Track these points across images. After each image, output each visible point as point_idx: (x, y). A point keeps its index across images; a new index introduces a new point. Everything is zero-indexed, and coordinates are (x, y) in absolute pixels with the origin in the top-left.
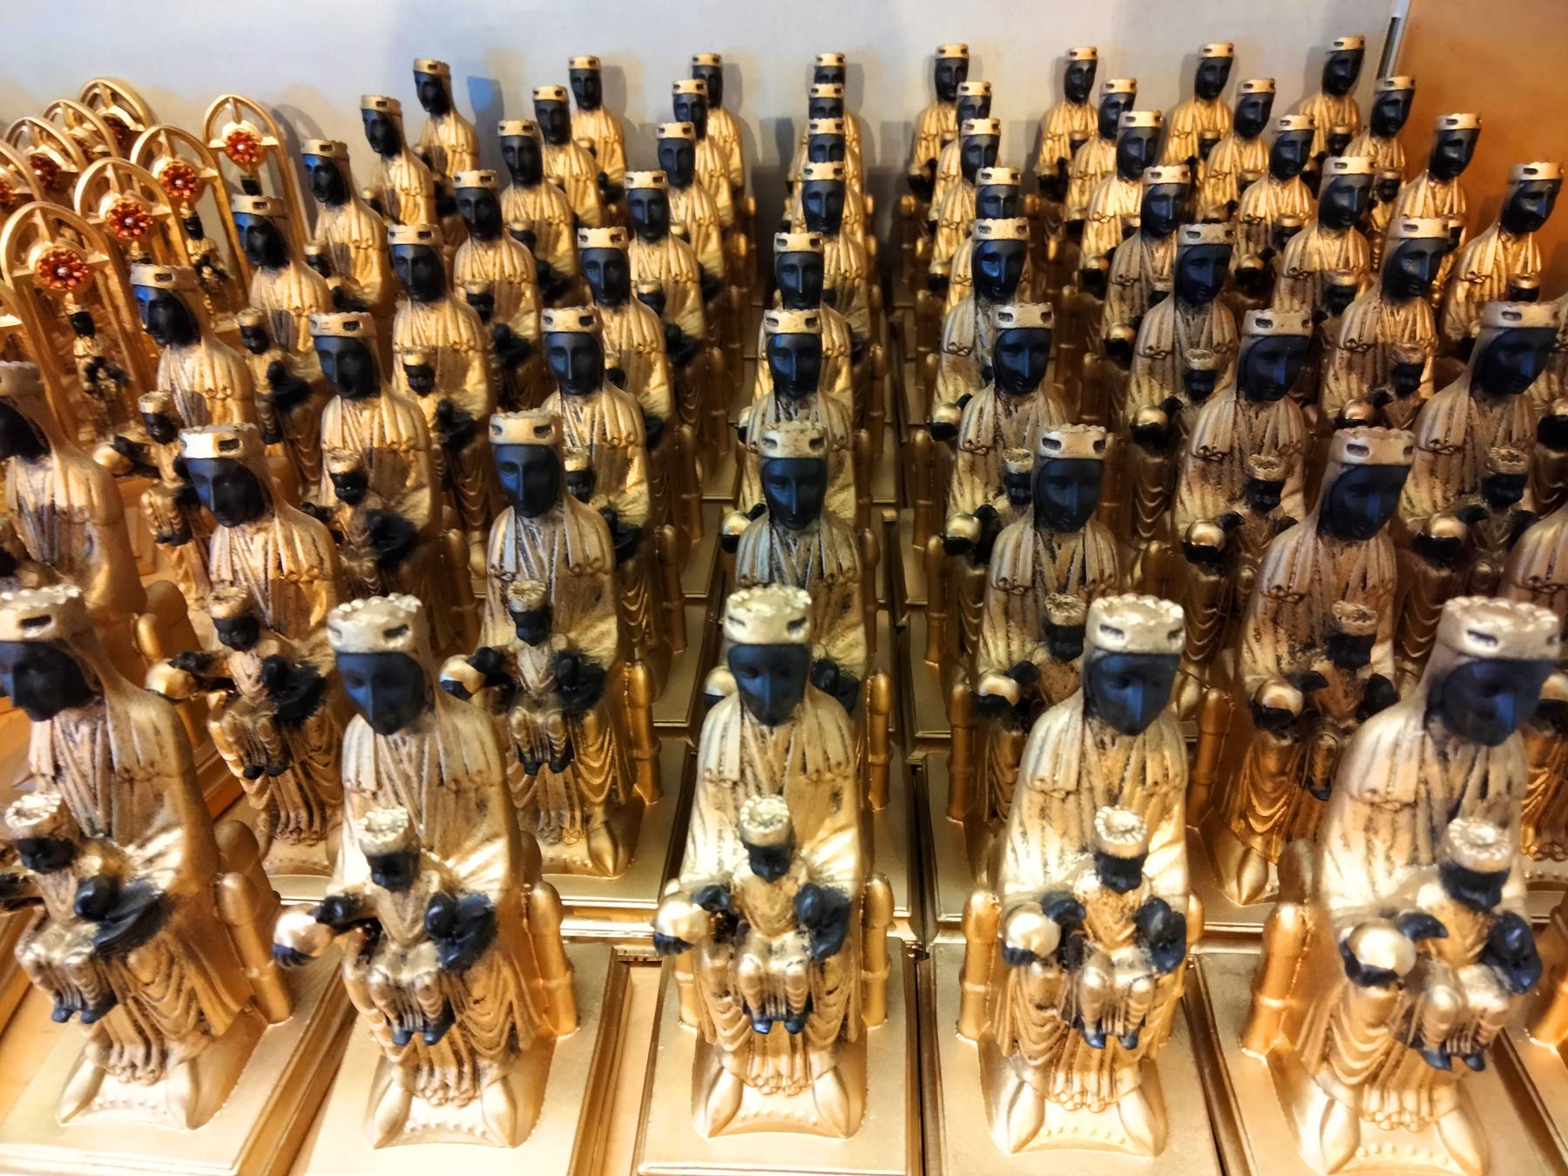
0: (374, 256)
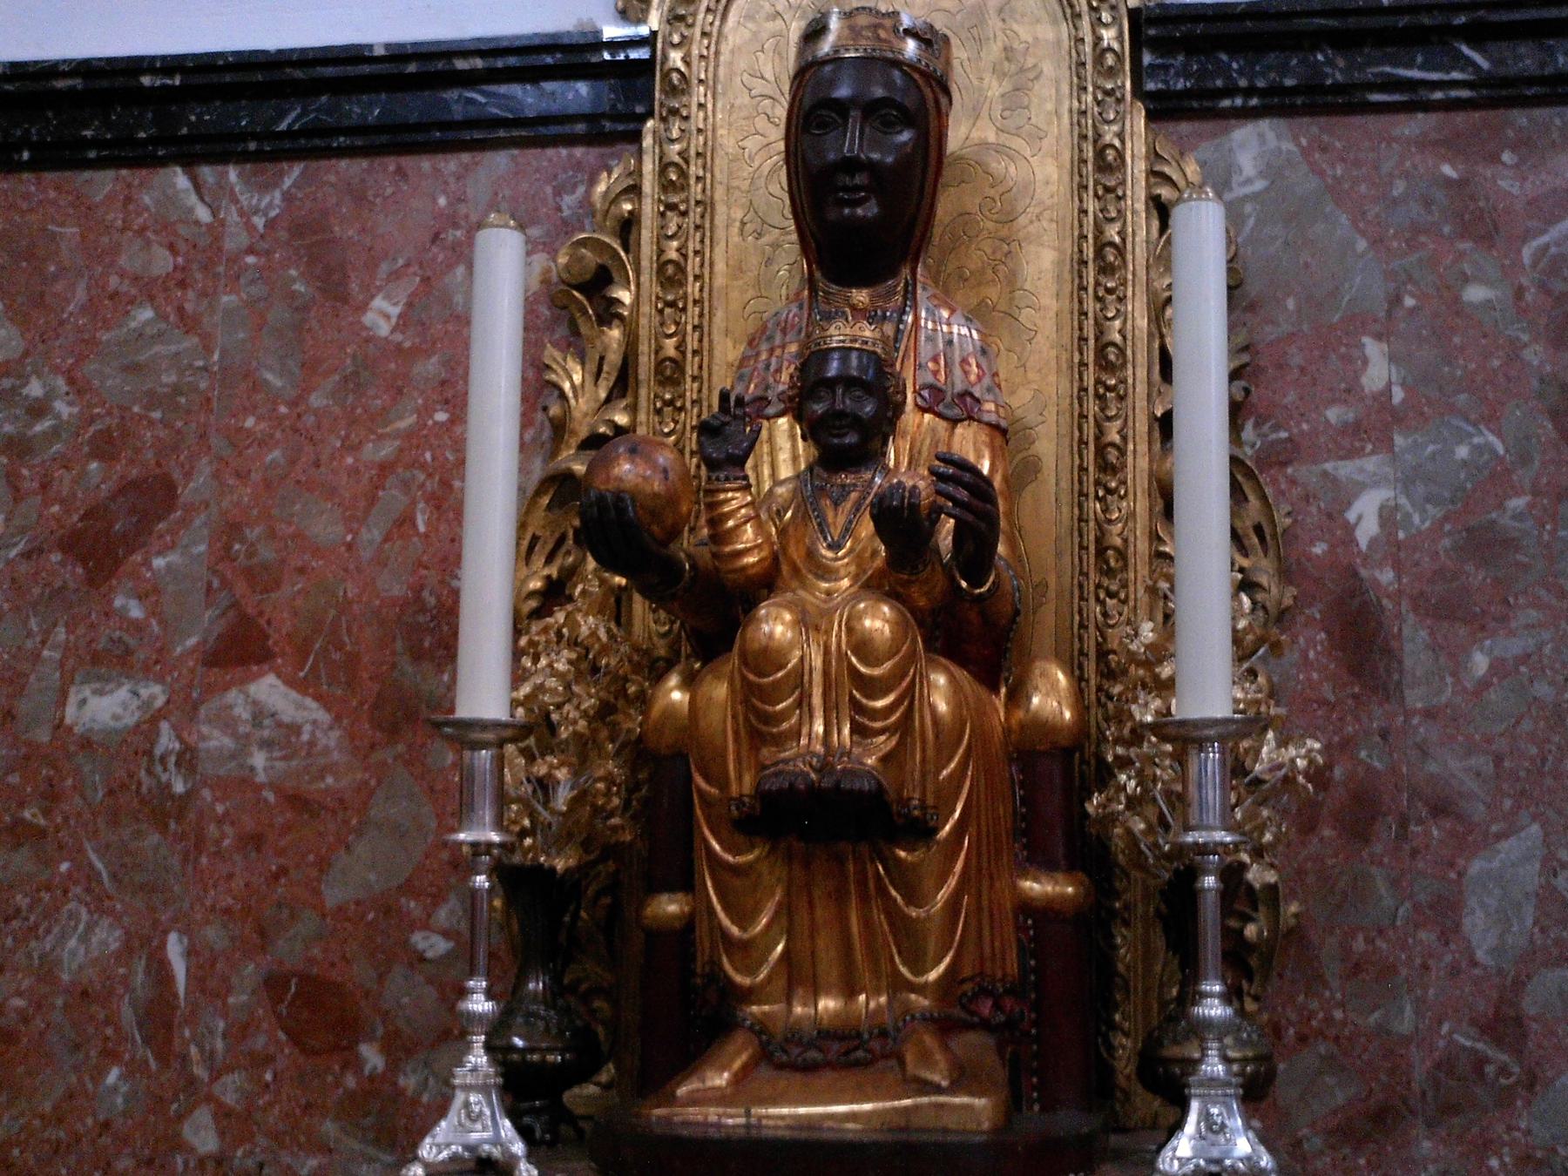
0: (1014, 946)
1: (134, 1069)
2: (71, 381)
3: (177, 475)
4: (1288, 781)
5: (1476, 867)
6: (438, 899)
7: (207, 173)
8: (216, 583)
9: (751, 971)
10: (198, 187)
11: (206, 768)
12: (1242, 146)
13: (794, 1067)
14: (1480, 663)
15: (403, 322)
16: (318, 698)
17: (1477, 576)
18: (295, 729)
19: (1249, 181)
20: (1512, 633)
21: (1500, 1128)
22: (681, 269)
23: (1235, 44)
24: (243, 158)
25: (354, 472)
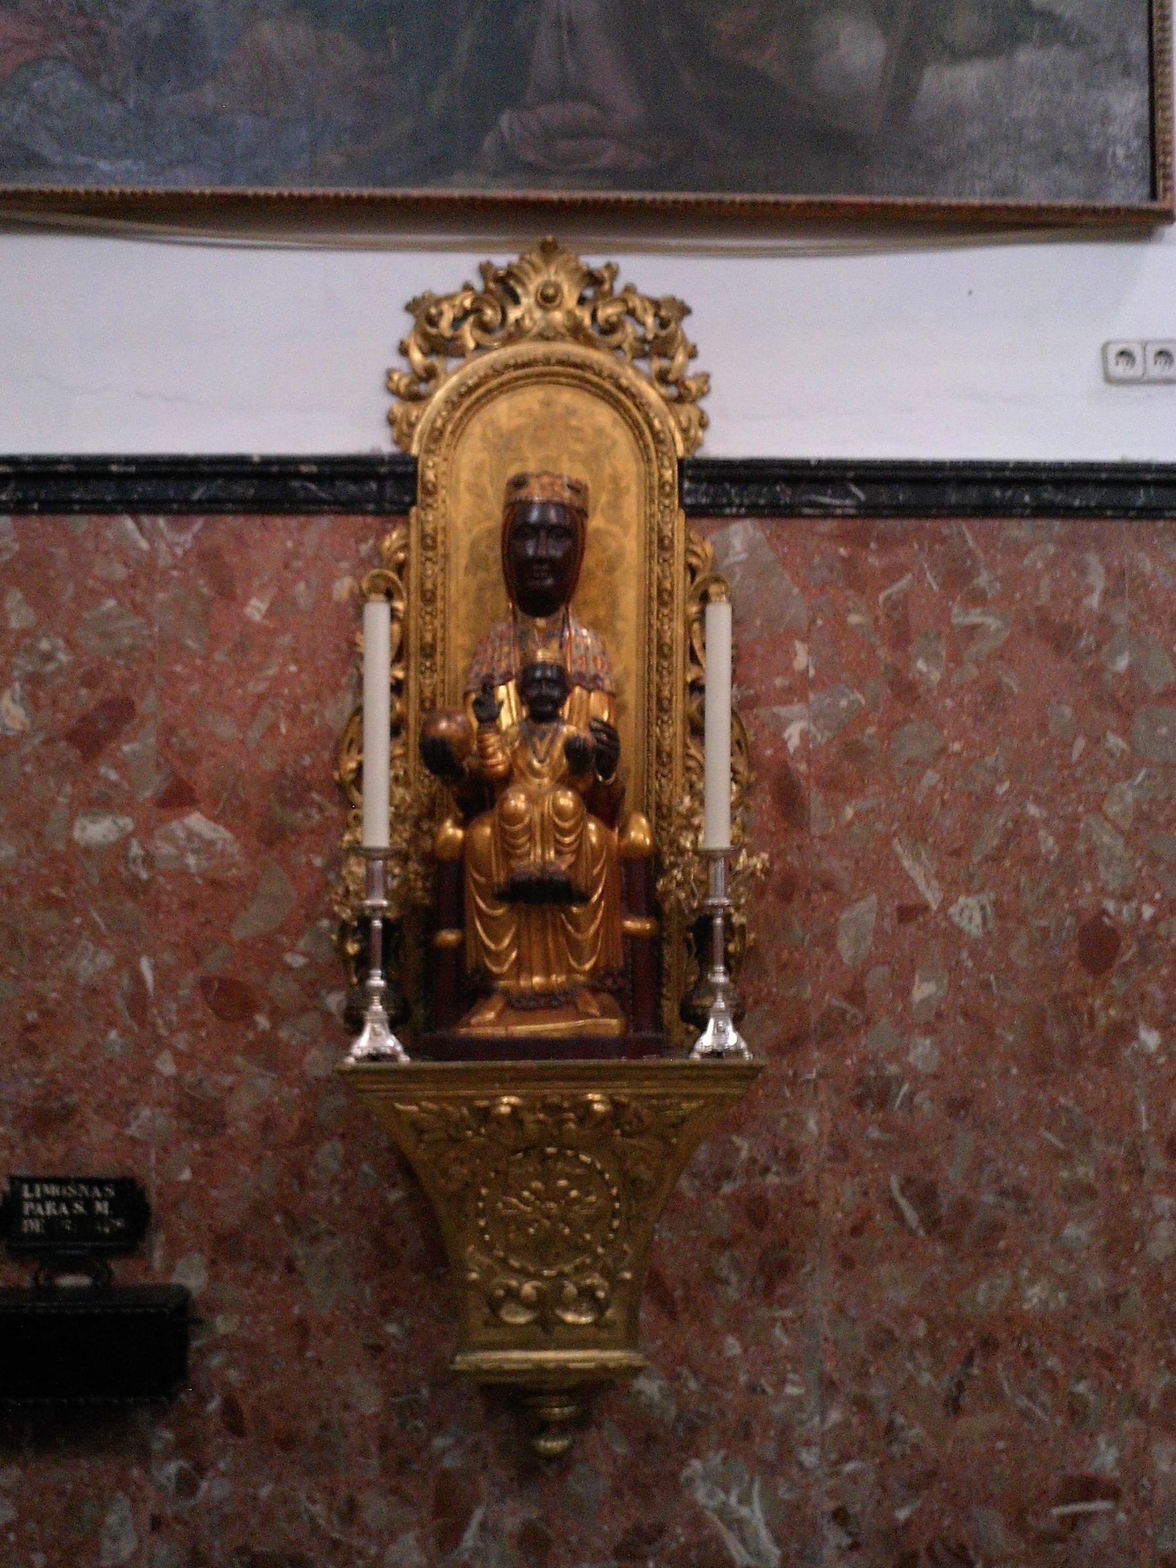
1: (125, 1031)
2: (67, 641)
3: (135, 699)
4: (753, 874)
5: (844, 916)
6: (298, 934)
7: (146, 520)
8: (162, 760)
9: (500, 964)
10: (141, 529)
11: (160, 865)
12: (736, 533)
13: (524, 1009)
14: (849, 812)
15: (269, 614)
16: (227, 826)
17: (849, 768)
18: (211, 843)
19: (738, 554)
20: (866, 798)
21: (852, 1045)
22: (434, 593)
23: (733, 481)
24: (168, 512)
25: (243, 699)
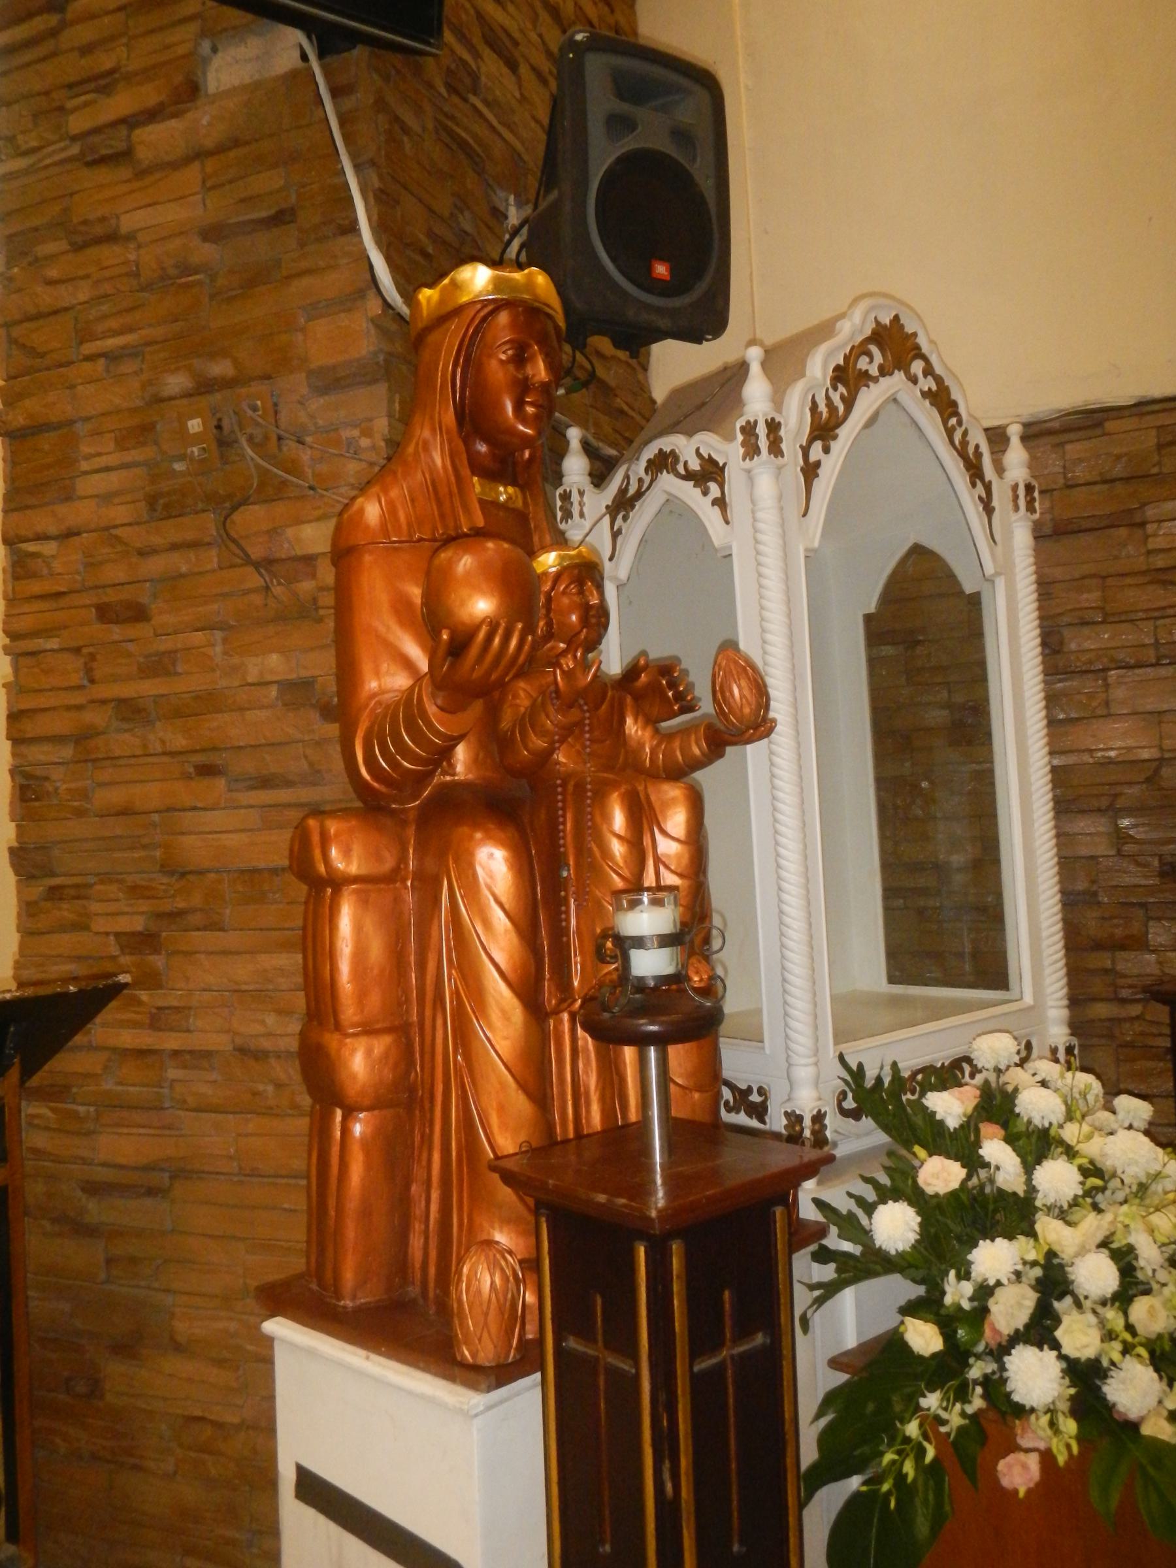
10: (338, 502)
